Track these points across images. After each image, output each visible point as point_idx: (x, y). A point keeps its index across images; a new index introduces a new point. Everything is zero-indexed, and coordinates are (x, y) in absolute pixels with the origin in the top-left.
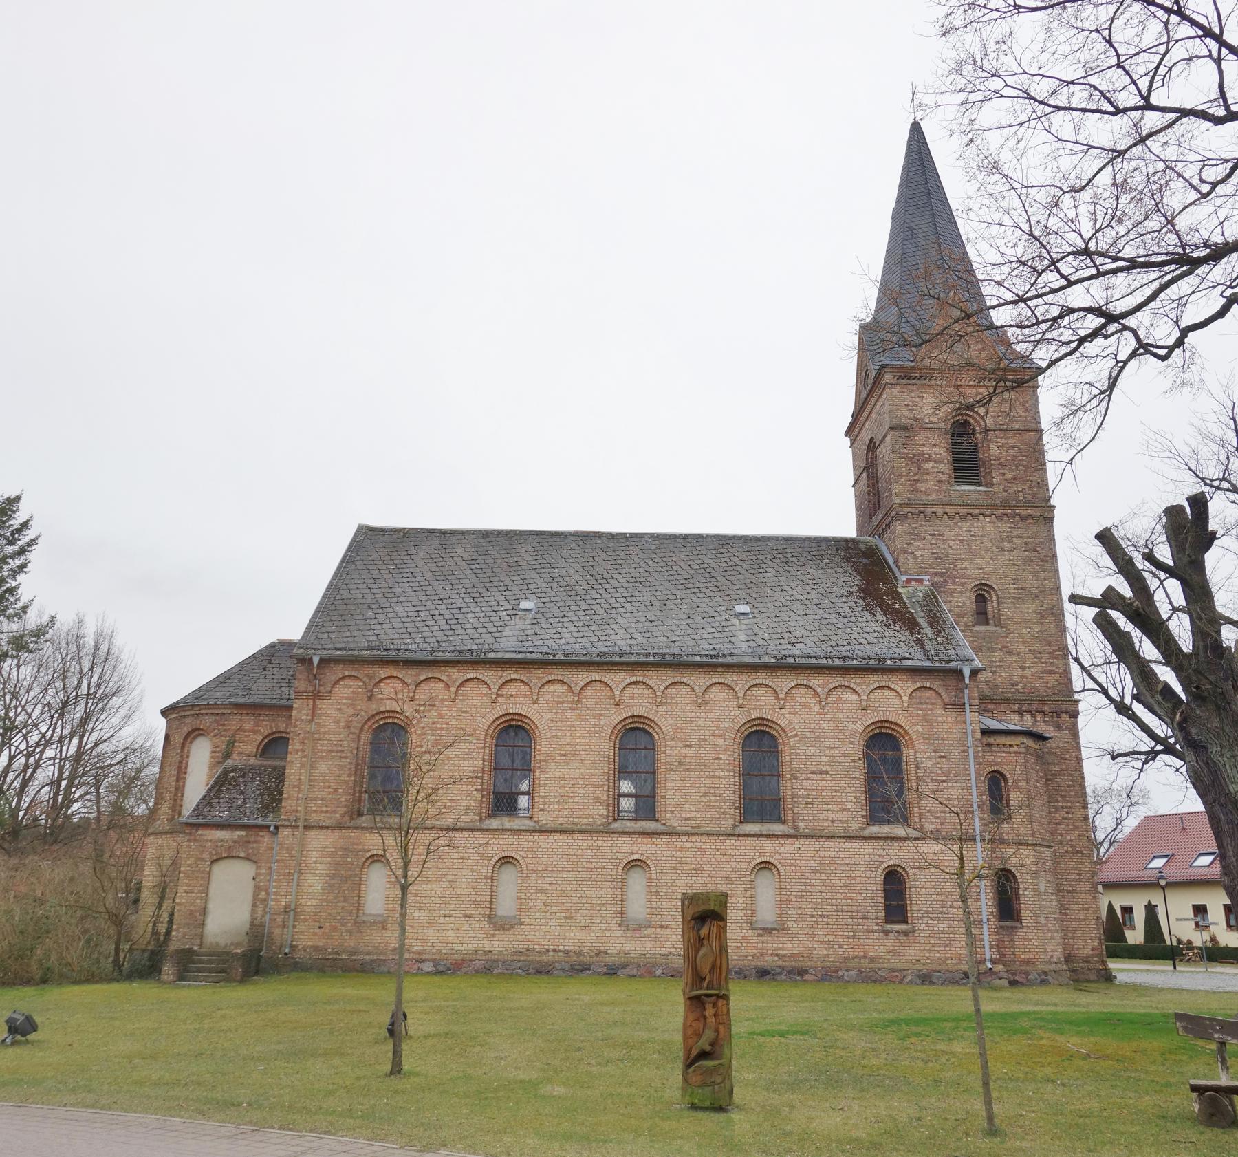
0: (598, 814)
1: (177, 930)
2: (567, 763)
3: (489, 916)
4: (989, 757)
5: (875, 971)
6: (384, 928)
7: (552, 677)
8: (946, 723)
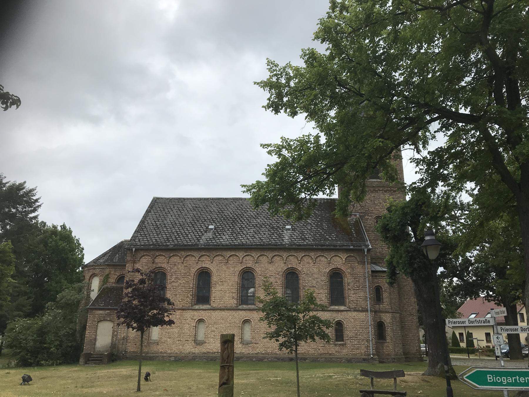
0: (233, 302)
1: (86, 346)
2: (223, 285)
3: (194, 341)
4: (376, 280)
5: (331, 358)
6: (158, 345)
7: (218, 254)
8: (359, 269)
